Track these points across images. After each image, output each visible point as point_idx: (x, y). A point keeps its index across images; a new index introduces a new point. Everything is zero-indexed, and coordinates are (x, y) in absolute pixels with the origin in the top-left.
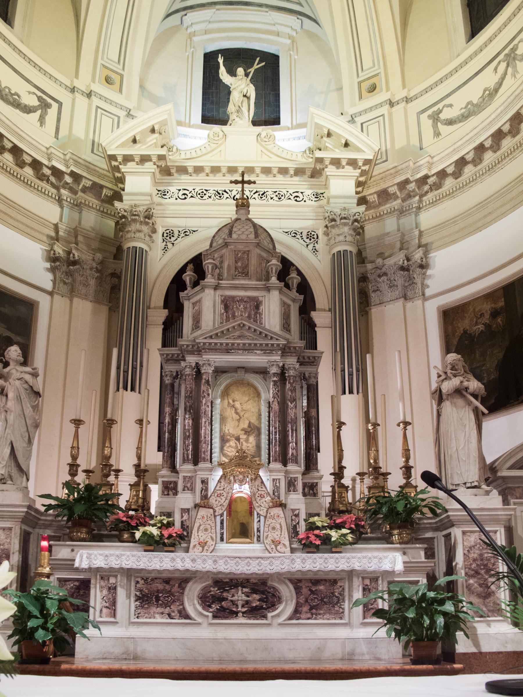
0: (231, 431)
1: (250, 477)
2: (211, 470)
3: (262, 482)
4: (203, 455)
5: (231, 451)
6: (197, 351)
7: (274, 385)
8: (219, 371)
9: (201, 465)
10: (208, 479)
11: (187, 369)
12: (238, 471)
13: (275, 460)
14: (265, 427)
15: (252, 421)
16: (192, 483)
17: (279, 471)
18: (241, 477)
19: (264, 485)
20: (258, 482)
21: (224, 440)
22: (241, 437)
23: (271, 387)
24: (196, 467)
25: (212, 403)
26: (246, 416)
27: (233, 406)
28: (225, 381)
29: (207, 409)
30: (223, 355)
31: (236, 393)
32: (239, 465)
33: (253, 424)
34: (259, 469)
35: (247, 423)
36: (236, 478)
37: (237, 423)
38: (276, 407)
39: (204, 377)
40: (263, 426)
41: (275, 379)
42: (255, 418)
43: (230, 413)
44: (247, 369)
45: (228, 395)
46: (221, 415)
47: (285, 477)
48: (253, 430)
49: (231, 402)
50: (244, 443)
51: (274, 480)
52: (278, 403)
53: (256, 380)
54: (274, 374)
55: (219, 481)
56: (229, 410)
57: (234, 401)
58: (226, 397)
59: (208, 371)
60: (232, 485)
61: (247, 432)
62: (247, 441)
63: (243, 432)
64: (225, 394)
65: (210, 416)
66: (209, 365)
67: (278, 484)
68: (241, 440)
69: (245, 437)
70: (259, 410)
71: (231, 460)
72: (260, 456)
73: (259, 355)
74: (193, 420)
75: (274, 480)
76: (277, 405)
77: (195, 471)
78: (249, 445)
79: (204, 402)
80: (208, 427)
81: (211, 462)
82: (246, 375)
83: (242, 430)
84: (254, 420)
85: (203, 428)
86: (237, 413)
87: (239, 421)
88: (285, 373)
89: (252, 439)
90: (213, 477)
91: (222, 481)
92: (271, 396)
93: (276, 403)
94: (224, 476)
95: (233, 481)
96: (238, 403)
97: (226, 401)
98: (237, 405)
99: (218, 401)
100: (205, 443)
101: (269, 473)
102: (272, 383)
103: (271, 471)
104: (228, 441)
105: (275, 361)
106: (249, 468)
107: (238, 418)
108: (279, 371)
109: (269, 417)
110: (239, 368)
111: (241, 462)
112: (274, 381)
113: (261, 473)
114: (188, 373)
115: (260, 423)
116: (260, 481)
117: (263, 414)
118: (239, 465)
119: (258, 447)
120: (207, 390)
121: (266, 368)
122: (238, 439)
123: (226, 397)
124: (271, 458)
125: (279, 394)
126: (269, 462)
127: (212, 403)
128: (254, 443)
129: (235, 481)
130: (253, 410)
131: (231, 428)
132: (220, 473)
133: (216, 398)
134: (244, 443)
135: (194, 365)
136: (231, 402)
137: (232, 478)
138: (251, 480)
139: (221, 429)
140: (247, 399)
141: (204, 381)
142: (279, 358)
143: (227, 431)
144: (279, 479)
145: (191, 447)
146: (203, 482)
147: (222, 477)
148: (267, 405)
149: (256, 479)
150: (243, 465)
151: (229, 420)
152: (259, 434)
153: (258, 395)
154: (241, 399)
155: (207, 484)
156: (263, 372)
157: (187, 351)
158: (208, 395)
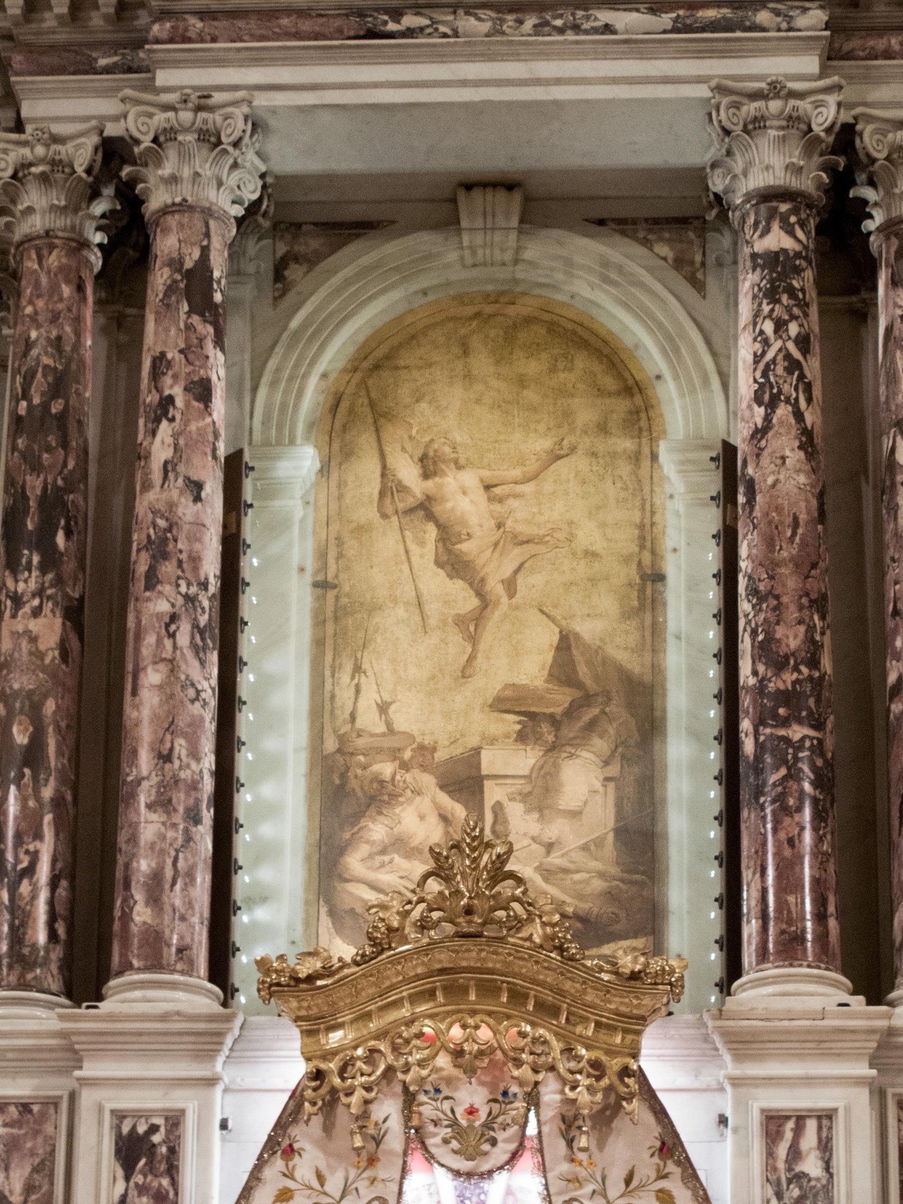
0: (407, 717)
1: (550, 1094)
2: (205, 1041)
3: (670, 1146)
4: (142, 914)
5: (389, 867)
6: (115, 47)
7: (772, 295)
8: (304, 227)
9: (130, 998)
10: (175, 1120)
11: (34, 197)
12: (436, 1044)
13: (790, 947)
14: (694, 672)
15: (588, 630)
16: (44, 1167)
17: (820, 1042)
18: (472, 1095)
19: (686, 1165)
20: (628, 1147)
21: (343, 796)
22: (489, 762)
23: (745, 308)
24: (85, 1020)
25: (234, 470)
26: (532, 583)
27: (426, 508)
28: (354, 307)
29: (187, 510)
30: (327, 56)
31: (454, 396)
32: (450, 986)
33: (595, 654)
34: (635, 1024)
35: (541, 640)
36: (428, 1109)
37: (456, 646)
38: (785, 476)
39: (166, 244)
40: (675, 660)
41: (777, 240)
42: (607, 603)
43: (399, 568)
44: (538, 200)
45: (381, 416)
46: (322, 585)
47: (879, 1095)
48: (595, 703)
49: (407, 472)
50: (515, 812)
51: (773, 1123)
52: (807, 442)
53: (613, 289)
54: (768, 197)
55: (279, 1144)
56: (388, 541)
57: (429, 466)
58: (366, 441)
59: (205, 196)
60: (387, 1171)
61: (545, 724)
62: (541, 793)
63: (512, 723)
64: (361, 406)
65: (211, 567)
66: (211, 139)
67: (812, 1166)
68: (493, 793)
69: (524, 760)
70: (647, 537)
71: (380, 942)
72: (649, 920)
73: (634, 47)
74: (73, 614)
75: (773, 1123)
76: (795, 456)
77: (69, 1053)
78: (557, 829)
79: (160, 449)
80: (191, 668)
81: (220, 970)
82: (533, 250)
83: (501, 704)
84: (600, 623)
85: (153, 677)
86: (455, 564)
87: (472, 626)
88: (861, 210)
89: (585, 781)
90: (220, 1104)
91: (305, 1136)
92: (745, 384)
93: (785, 443)
94: (319, 1096)
95: (395, 1140)
96: (470, 478)
97: (365, 473)
98: (462, 495)
99: (301, 463)
100: (163, 803)
101: (729, 1066)
102: (749, 281)
103: (744, 1044)
104: (380, 797)
105: (776, 90)
106: (547, 1010)
107: (469, 602)
108: (810, 180)
109: (728, 574)
110: (469, 187)
111: (472, 955)
112: (773, 262)
113: (661, 1060)
114: (36, 224)
115: (655, 636)
116: (652, 1131)
117: (675, 570)
118: (455, 991)
119: (640, 842)
120: (192, 351)
121: (697, 177)
122: (464, 780)
123: (366, 441)
124: (750, 929)
125: (813, 367)
126: (733, 968)
127: (234, 470)
128: (602, 816)
129: (417, 1137)
130: (589, 535)
131: (409, 692)
132: (279, 1066)
133: (281, 440)
134: (515, 812)
135: (82, 155)
136: (407, 472)
137: (388, 1110)
138: (569, 1124)
139: (320, 708)
140: (542, 444)
141: (160, 278)
142: (810, 64)
143: (369, 720)
144: (826, 1117)
145: (46, 849)
146: (133, 1150)
147: (297, 1098)
148: (714, 483)
149: (607, 1116)
150: (489, 990)
151: (393, 624)
152: (649, 726)
153: (631, 398)
154: (483, 445)
155: (172, 1170)
156: (675, 219)
157: (30, 49)
158: (202, 391)
